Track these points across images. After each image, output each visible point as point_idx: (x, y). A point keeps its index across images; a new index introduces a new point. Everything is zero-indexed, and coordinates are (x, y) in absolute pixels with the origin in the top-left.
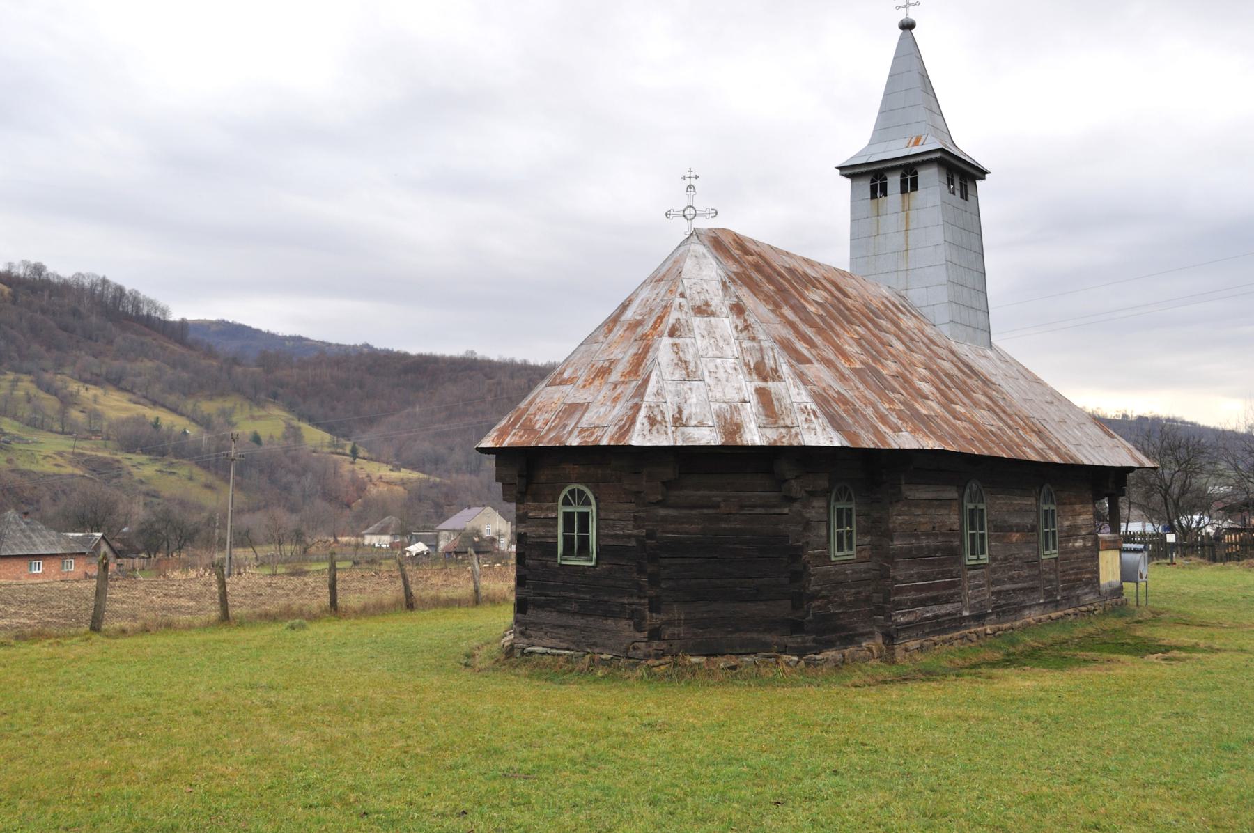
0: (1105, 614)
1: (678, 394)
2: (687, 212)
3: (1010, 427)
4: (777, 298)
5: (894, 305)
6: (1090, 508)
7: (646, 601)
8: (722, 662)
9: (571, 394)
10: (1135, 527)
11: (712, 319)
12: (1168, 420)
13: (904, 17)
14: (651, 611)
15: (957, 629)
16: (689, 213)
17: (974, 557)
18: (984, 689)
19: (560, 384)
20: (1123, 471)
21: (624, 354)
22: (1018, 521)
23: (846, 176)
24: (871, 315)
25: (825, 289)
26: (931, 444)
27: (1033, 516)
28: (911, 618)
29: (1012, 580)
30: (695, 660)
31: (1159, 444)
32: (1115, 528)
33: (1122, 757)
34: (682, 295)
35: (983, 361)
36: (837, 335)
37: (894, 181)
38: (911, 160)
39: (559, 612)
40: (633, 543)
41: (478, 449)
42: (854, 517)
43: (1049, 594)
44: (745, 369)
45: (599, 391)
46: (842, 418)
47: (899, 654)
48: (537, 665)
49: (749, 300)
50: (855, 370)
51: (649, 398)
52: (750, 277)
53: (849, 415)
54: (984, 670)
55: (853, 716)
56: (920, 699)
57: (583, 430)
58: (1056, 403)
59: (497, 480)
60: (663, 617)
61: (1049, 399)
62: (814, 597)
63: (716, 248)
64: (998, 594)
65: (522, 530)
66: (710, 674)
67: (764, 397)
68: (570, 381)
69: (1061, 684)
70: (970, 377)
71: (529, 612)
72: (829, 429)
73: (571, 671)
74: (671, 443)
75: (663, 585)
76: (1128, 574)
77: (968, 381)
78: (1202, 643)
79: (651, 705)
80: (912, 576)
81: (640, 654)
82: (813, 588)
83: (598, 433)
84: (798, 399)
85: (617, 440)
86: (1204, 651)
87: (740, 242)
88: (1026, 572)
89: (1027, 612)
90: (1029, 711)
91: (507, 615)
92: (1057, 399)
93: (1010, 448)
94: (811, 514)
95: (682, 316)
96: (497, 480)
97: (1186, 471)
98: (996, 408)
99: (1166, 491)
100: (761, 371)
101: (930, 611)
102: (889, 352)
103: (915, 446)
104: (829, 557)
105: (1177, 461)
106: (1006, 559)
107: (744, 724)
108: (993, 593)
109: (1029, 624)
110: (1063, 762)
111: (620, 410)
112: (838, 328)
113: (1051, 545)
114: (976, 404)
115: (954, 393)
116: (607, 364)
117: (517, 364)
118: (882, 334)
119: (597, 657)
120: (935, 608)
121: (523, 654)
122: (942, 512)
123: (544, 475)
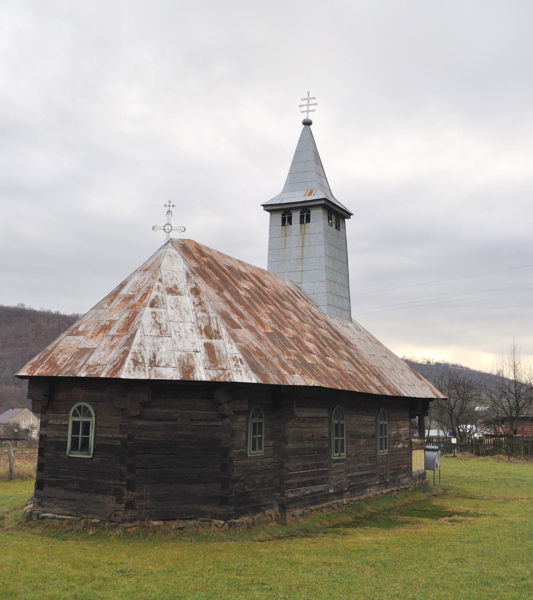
0: (415, 490)
1: (154, 345)
2: (166, 228)
3: (361, 372)
4: (221, 285)
5: (293, 292)
6: (407, 423)
7: (125, 483)
8: (174, 525)
9: (82, 342)
10: (433, 433)
11: (179, 297)
12: (453, 365)
13: (306, 118)
14: (128, 490)
15: (325, 501)
16: (167, 228)
17: (337, 454)
18: (341, 543)
19: (76, 335)
20: (426, 402)
21: (120, 317)
22: (364, 431)
23: (267, 210)
24: (278, 298)
25: (251, 281)
26: (313, 382)
27: (374, 428)
28: (297, 494)
29: (360, 469)
30: (156, 523)
31: (447, 383)
32: (422, 435)
33: (424, 590)
34: (160, 280)
35: (346, 330)
36: (258, 311)
37: (296, 216)
38: (312, 204)
39: (66, 489)
40: (118, 443)
41: (16, 376)
42: (263, 428)
43: (382, 478)
44: (198, 331)
45: (102, 340)
46: (258, 364)
47: (289, 518)
48: (48, 526)
49: (203, 286)
50: (267, 334)
51: (134, 347)
52: (204, 271)
53: (262, 362)
54: (341, 529)
55: (257, 563)
56: (301, 550)
57: (89, 367)
58: (389, 357)
59: (29, 398)
60: (137, 494)
61: (385, 355)
62: (236, 481)
63: (183, 251)
64: (351, 478)
65: (44, 433)
66: (165, 533)
67: (209, 349)
68: (83, 333)
69: (388, 539)
70: (338, 340)
71: (45, 488)
72: (250, 372)
73: (71, 531)
74: (147, 377)
75: (137, 472)
76: (429, 465)
77: (337, 342)
78: (472, 510)
79: (124, 556)
80: (298, 467)
81: (119, 519)
82: (235, 475)
83: (99, 369)
84: (231, 351)
85: (112, 374)
86: (472, 515)
87: (199, 249)
88: (368, 464)
89: (368, 490)
90: (368, 558)
91: (28, 489)
92: (389, 354)
93: (361, 386)
94: (236, 426)
95: (159, 294)
96: (29, 398)
97: (463, 399)
98: (353, 360)
99: (452, 411)
100: (208, 332)
101: (309, 490)
102: (289, 323)
103: (303, 383)
104: (247, 455)
105: (458, 393)
106: (356, 456)
107: (186, 570)
108: (348, 478)
109: (370, 497)
110: (388, 595)
111: (115, 354)
112: (258, 306)
113: (384, 447)
114: (341, 357)
115: (328, 350)
116: (108, 323)
117: (52, 314)
118: (285, 311)
119: (89, 520)
120: (312, 487)
121: (38, 518)
122: (319, 425)
123: (60, 396)
